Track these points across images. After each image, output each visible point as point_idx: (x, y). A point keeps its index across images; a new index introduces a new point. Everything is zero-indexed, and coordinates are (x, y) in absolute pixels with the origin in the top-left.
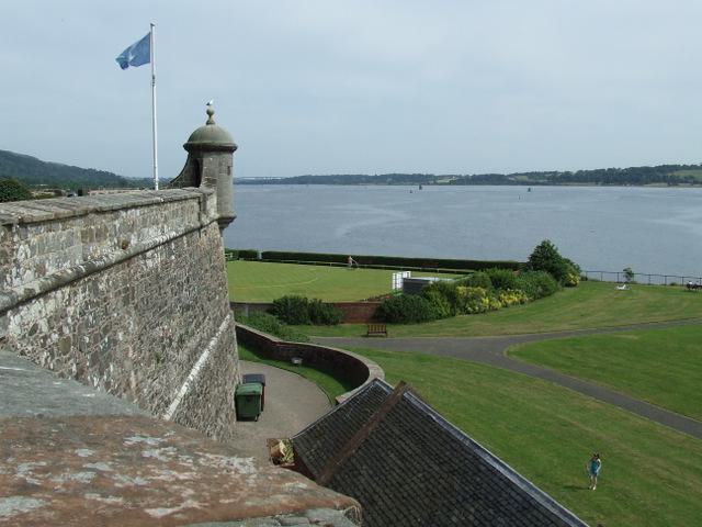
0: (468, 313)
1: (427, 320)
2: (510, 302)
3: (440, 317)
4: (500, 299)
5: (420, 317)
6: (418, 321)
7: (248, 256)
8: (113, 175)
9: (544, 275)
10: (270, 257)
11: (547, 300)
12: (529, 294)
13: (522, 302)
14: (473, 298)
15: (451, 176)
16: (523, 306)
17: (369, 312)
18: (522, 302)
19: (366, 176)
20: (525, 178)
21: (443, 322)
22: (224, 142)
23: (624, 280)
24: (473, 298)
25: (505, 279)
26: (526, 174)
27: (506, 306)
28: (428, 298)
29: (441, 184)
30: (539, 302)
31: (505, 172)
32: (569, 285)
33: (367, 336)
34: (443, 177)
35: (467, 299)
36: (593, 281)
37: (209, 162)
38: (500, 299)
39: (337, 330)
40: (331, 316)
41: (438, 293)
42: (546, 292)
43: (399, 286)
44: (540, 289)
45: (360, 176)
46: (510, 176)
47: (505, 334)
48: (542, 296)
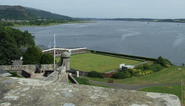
0: (136, 76)
1: (124, 78)
2: (147, 73)
3: (128, 77)
4: (145, 72)
5: (123, 77)
6: (122, 79)
7: (92, 52)
8: (69, 17)
9: (159, 65)
10: (98, 53)
11: (158, 72)
12: (153, 71)
13: (151, 73)
14: (137, 72)
15: (158, 19)
16: (151, 74)
17: (111, 76)
18: (151, 73)
19: (134, 19)
20: (179, 21)
21: (128, 79)
22: (66, 57)
23: (182, 66)
24: (137, 72)
25: (147, 67)
26: (179, 19)
27: (146, 74)
28: (125, 73)
29: (155, 22)
30: (156, 73)
31: (173, 19)
32: (166, 67)
33: (109, 82)
34: (155, 20)
35: (136, 73)
36: (174, 65)
37: (64, 60)
38: (145, 72)
39: (103, 80)
40: (102, 76)
41: (128, 72)
42: (158, 70)
43: (121, 67)
44: (157, 69)
45: (133, 19)
46: (174, 20)
47: (141, 84)
48: (157, 71)
